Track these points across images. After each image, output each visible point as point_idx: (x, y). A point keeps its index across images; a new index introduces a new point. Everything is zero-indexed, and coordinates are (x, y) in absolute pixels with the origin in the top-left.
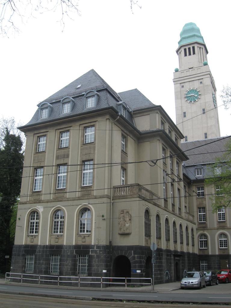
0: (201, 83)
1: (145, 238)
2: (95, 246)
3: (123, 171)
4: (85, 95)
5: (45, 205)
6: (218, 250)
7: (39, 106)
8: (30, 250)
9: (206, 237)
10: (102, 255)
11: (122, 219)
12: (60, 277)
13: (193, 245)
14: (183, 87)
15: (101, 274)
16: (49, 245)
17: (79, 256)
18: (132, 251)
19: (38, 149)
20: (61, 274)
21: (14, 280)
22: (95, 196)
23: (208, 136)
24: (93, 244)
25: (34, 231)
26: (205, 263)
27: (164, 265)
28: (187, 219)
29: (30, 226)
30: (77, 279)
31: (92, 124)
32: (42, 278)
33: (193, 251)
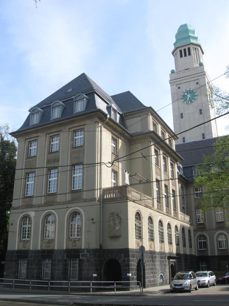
0: (197, 83)
1: (136, 241)
2: (86, 250)
3: (114, 173)
4: (74, 99)
5: (37, 209)
6: (218, 251)
7: (30, 112)
8: (22, 254)
9: (205, 238)
10: (92, 258)
11: (112, 222)
12: (50, 282)
13: (191, 247)
14: (179, 88)
15: (92, 278)
16: (41, 249)
17: (70, 261)
18: (123, 255)
19: (29, 154)
20: (52, 278)
21: (8, 286)
22: (85, 200)
23: (205, 136)
24: (83, 248)
25: (27, 236)
26: (205, 264)
27: (158, 267)
28: (183, 220)
29: (22, 231)
30: (67, 284)
31: (81, 127)
32: (34, 283)
33: (190, 252)
